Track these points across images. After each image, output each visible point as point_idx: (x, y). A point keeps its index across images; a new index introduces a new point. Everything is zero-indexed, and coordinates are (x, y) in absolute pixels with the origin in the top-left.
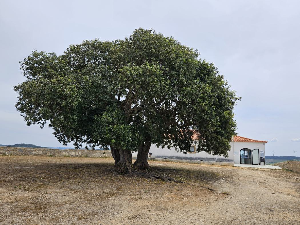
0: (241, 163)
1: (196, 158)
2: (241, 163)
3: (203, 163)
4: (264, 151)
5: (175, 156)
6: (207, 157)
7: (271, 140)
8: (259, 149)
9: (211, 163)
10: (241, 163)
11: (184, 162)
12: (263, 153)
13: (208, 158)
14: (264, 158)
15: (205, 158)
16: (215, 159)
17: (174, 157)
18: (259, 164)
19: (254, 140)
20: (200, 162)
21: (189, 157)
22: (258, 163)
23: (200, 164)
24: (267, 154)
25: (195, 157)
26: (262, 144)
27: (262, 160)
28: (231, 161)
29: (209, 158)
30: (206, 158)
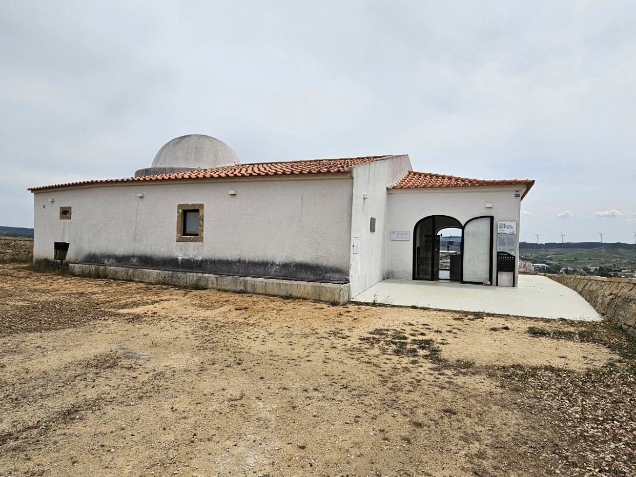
0: (414, 278)
1: (202, 261)
2: (498, 253)
3: (215, 285)
4: (514, 225)
5: (136, 253)
6: (242, 259)
7: (560, 215)
8: (492, 218)
9: (245, 282)
10: (498, 253)
11: (152, 280)
12: (507, 231)
13: (244, 262)
14: (516, 253)
15: (235, 262)
16: (273, 264)
17: (134, 256)
18: (492, 281)
19: (463, 180)
20: (207, 280)
21: (180, 257)
22: (483, 275)
23: (204, 289)
24: (527, 236)
25: (200, 258)
26: (508, 195)
27: (505, 264)
28: (337, 276)
29: (250, 262)
30: (239, 261)
